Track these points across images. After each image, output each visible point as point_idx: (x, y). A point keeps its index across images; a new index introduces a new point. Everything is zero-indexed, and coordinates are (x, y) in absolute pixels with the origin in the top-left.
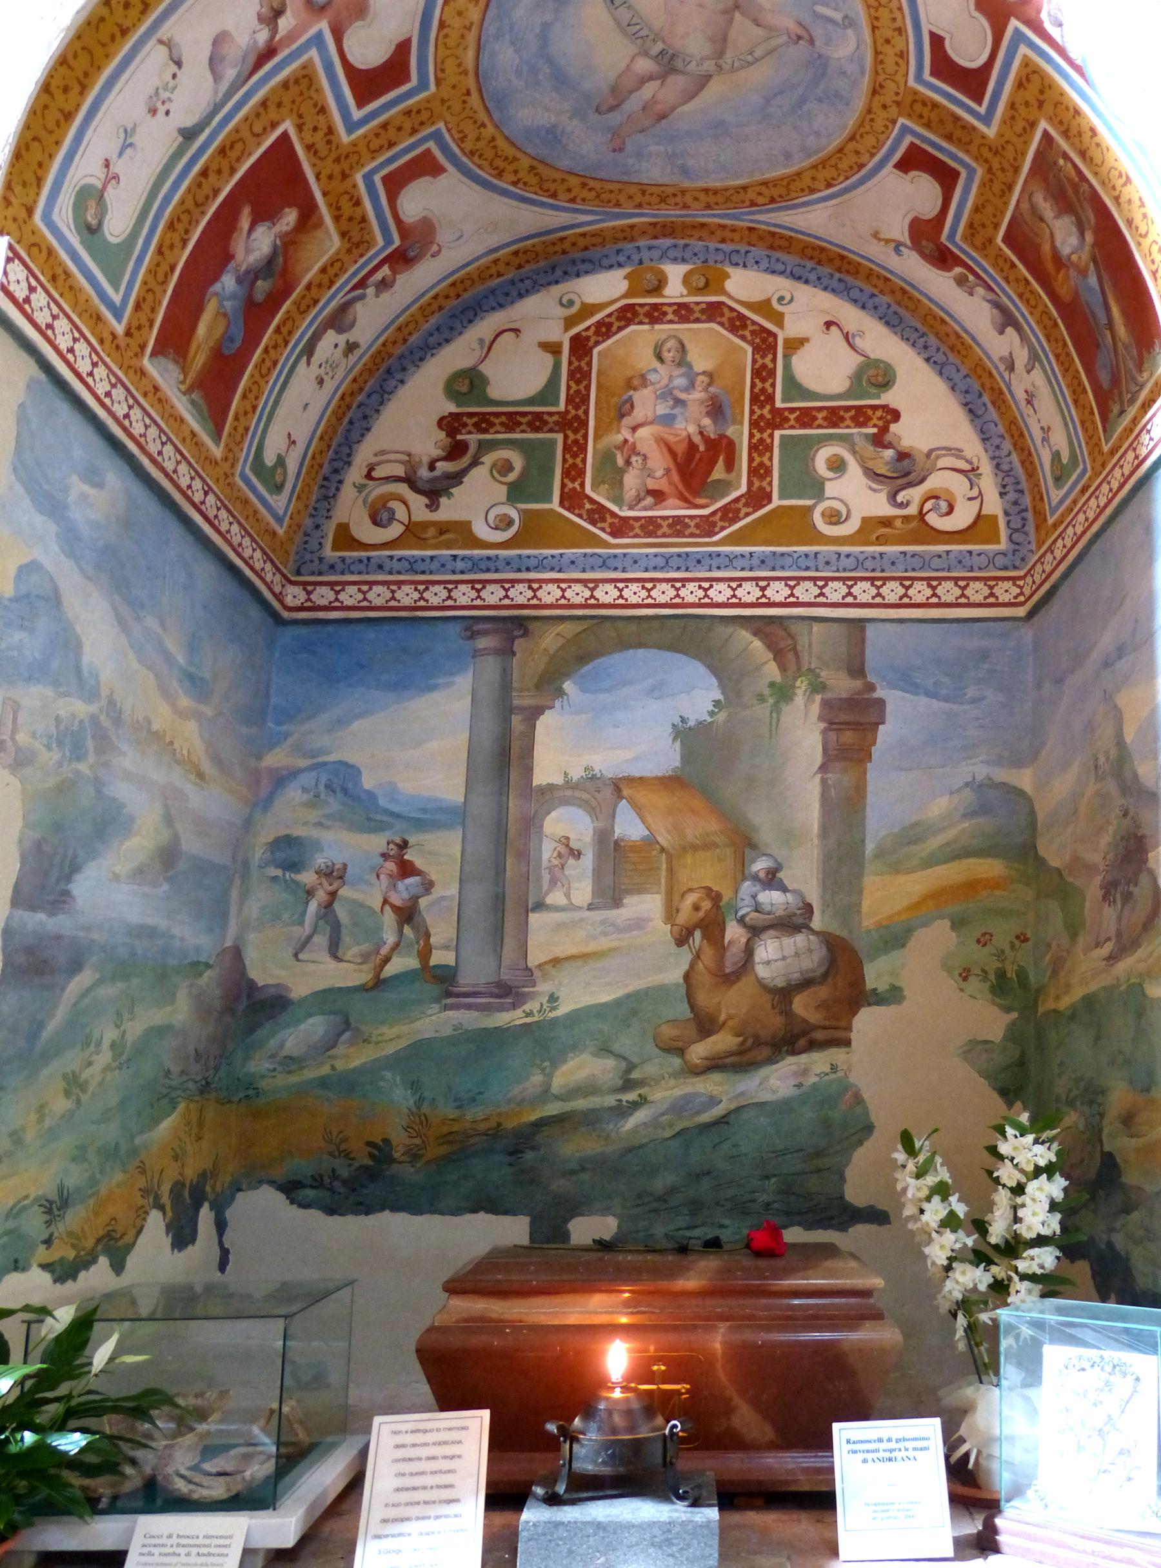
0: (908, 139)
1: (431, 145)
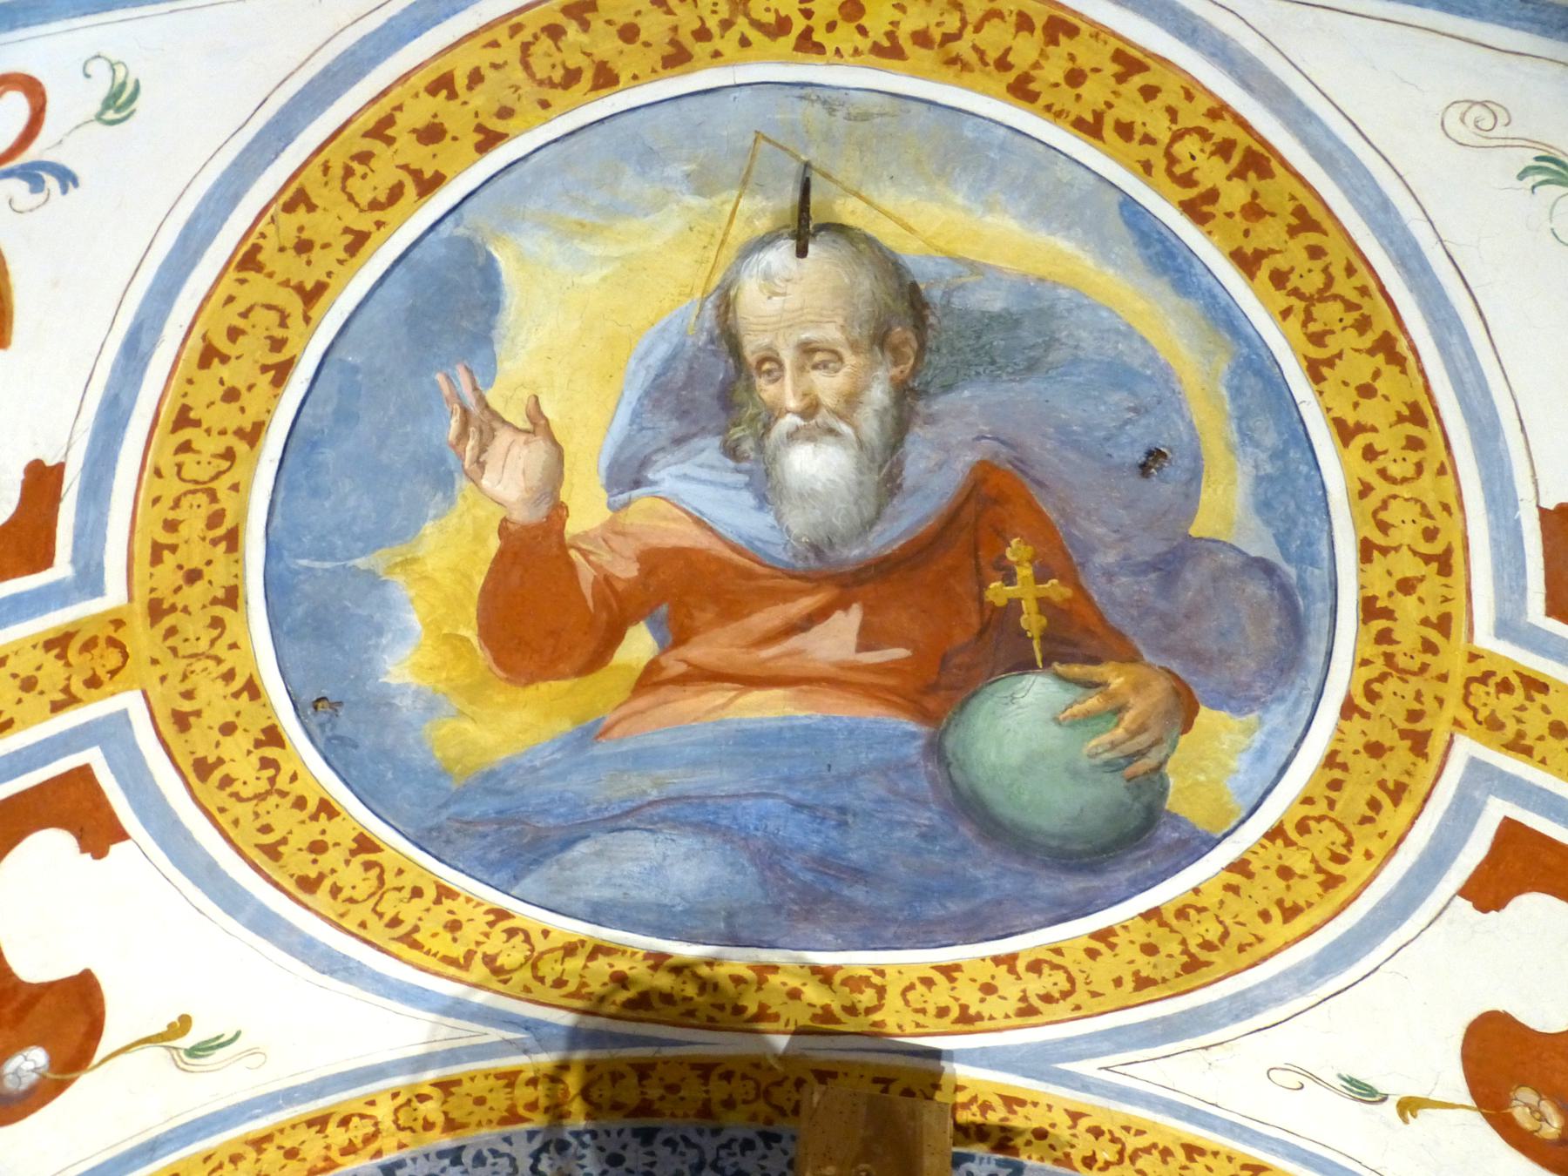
0: (1496, 810)
1: (93, 757)
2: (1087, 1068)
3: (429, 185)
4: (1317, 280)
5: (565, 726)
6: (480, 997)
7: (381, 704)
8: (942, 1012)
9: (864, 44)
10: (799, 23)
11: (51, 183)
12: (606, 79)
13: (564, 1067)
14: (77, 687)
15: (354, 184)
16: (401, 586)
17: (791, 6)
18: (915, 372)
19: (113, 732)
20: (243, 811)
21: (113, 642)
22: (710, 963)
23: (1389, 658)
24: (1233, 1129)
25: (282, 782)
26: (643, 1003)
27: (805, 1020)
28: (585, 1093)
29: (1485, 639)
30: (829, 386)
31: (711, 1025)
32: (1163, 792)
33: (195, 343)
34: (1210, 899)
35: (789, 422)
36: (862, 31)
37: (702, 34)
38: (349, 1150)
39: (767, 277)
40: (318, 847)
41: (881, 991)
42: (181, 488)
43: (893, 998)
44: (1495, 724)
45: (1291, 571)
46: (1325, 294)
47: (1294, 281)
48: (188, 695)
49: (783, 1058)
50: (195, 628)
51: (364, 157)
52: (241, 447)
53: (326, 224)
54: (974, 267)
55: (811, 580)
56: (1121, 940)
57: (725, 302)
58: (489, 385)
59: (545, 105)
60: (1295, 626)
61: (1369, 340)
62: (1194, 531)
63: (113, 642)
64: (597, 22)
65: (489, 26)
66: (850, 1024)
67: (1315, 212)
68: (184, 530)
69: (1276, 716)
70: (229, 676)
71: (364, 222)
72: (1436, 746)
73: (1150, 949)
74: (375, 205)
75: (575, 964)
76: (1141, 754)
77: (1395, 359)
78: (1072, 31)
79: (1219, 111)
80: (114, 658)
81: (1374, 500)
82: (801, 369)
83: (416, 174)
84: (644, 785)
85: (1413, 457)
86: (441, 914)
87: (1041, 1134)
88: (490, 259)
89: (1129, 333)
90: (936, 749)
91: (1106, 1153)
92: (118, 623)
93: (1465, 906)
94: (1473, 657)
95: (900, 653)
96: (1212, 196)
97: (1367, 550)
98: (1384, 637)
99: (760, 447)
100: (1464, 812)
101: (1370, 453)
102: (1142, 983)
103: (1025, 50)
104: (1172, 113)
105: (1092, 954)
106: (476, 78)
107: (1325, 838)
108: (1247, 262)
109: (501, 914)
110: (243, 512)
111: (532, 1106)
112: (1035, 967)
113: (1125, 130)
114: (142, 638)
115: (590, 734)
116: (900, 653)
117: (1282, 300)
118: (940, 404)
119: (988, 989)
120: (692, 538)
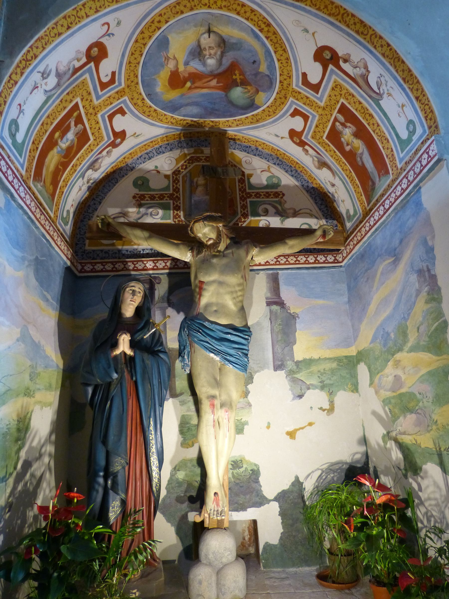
0: (294, 106)
1: (122, 105)
2: (245, 132)
3: (159, 29)
4: (276, 41)
5: (180, 94)
6: (170, 126)
7: (156, 94)
8: (227, 125)
9: (217, 7)
10: (208, 4)
11: (111, 35)
12: (182, 12)
13: (181, 133)
14: (120, 97)
15: (150, 29)
16: (158, 80)
17: (207, 2)
18: (224, 50)
19: (124, 102)
20: (140, 108)
21: (123, 91)
22: (198, 121)
23: (283, 88)
24: (262, 139)
25: (145, 104)
26: (190, 126)
27: (210, 126)
28: (183, 136)
29: (294, 86)
30: (212, 52)
31: (199, 127)
32: (254, 101)
33: (131, 53)
34: (260, 114)
35: (207, 56)
36: (217, 5)
37: (195, 6)
38: (156, 144)
39: (204, 38)
40: (150, 111)
41: (219, 123)
42: (130, 71)
43: (221, 124)
44: (295, 97)
45: (271, 76)
46: (277, 43)
47: (273, 41)
48: (133, 96)
49: (207, 131)
50: (133, 88)
51: (151, 26)
52: (137, 65)
53: (146, 35)
54: (232, 37)
55: (210, 76)
56: (249, 118)
57: (199, 41)
58: (168, 53)
59: (174, 17)
60: (271, 83)
61: (282, 49)
62: (259, 71)
63: (123, 91)
64: (181, 5)
65: (166, 7)
66: (216, 127)
67: (276, 33)
68: (131, 76)
69: (269, 93)
70: (137, 93)
71: (151, 34)
72: (288, 98)
73: (252, 119)
74: (152, 32)
75: (182, 122)
76: (252, 97)
77: (285, 52)
78: (245, 6)
79: (264, 18)
80: (124, 93)
81: (282, 69)
82: (209, 50)
83: (157, 27)
84: (190, 101)
85: (287, 64)
86: (165, 117)
87: (239, 139)
88: (168, 38)
89: (252, 46)
90: (226, 96)
91: (246, 141)
92: (124, 89)
93: (290, 117)
94: (293, 89)
95: (222, 84)
96: (263, 29)
97: (281, 75)
98: (282, 85)
99: (204, 60)
100: (290, 106)
101: (282, 63)
102: (251, 123)
103: (239, 8)
104: (258, 18)
105: (245, 119)
106: (165, 14)
107: (274, 108)
108: (267, 38)
109: (172, 117)
110: (138, 73)
111: (177, 138)
112: (238, 121)
113: (252, 20)
114: (127, 90)
115: (183, 95)
116: (222, 84)
117: (271, 43)
118: (227, 54)
119: (233, 123)
120: (195, 71)
